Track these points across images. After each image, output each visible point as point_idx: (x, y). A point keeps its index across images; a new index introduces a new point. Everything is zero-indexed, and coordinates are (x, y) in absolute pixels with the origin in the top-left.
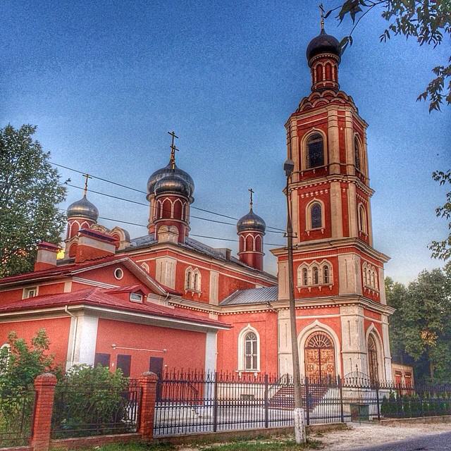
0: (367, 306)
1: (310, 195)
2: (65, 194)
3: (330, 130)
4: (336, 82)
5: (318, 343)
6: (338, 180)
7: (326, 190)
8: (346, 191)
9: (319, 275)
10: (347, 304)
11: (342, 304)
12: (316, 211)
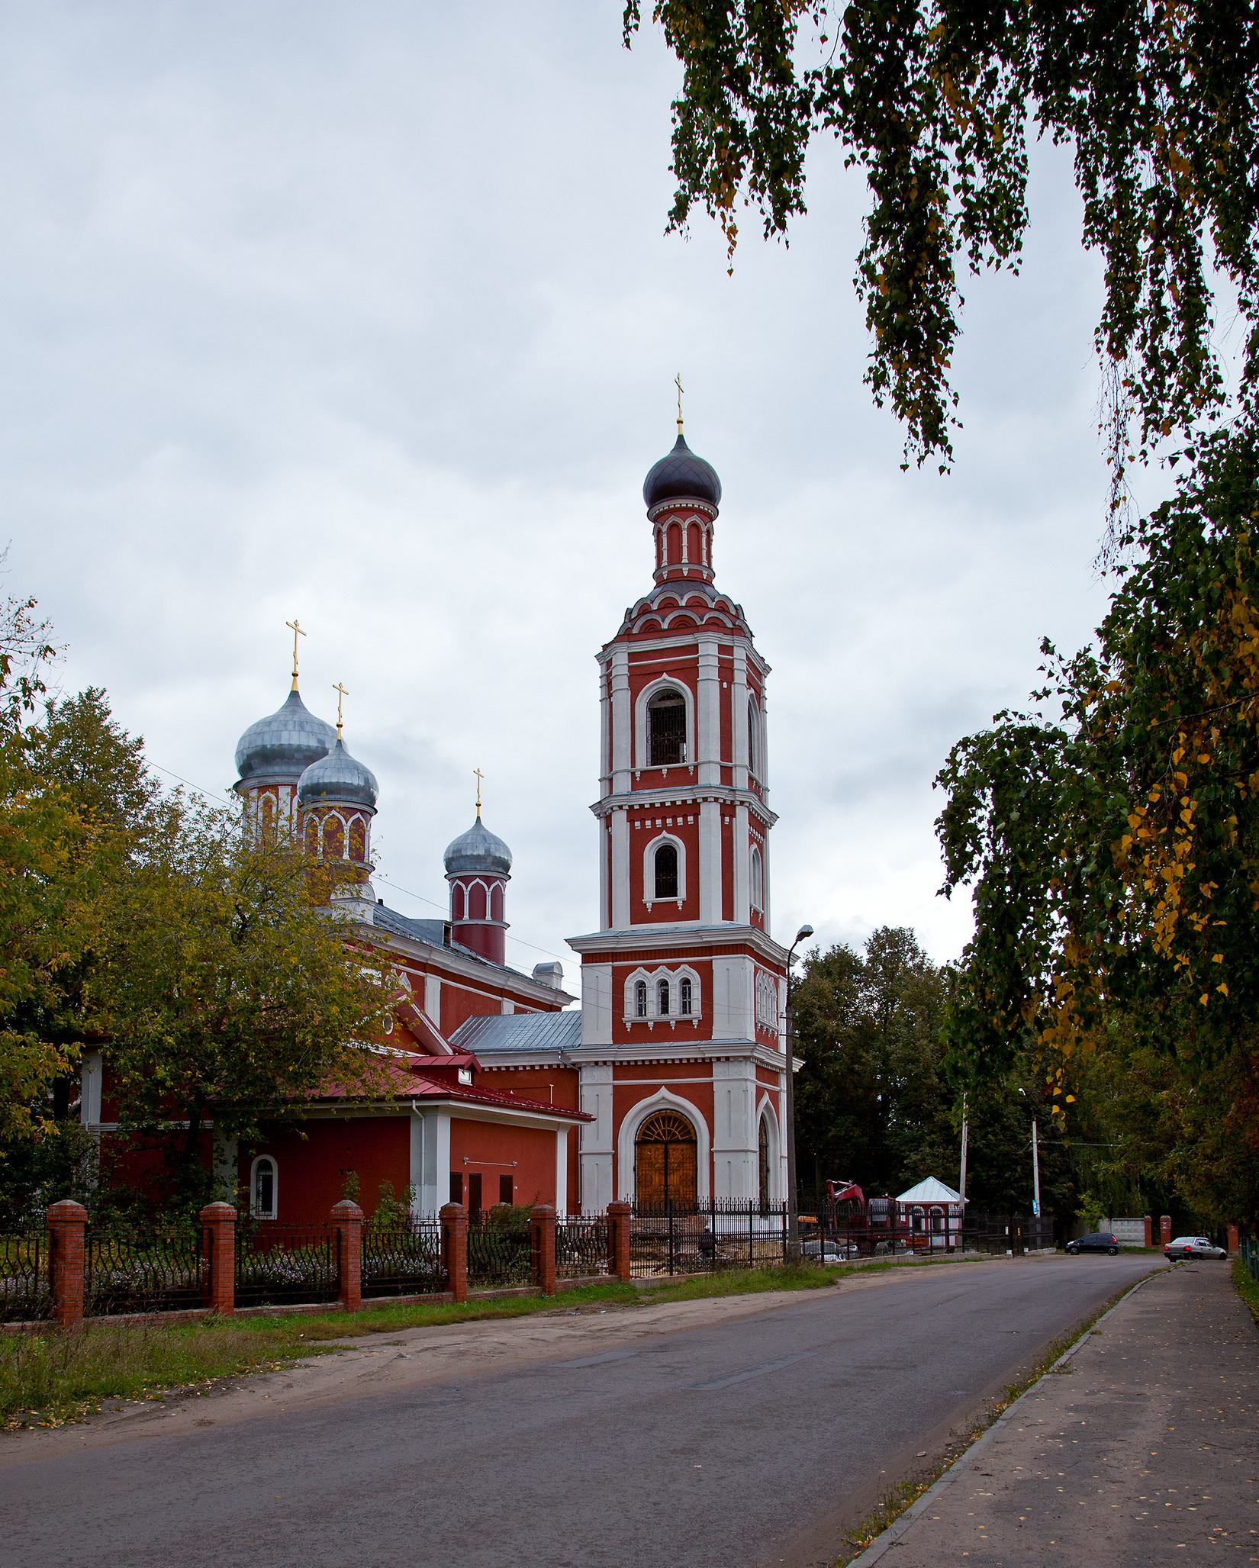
0: (762, 1061)
1: (654, 824)
2: (833, 128)
3: (700, 685)
4: (710, 567)
5: (663, 1131)
6: (716, 800)
7: (690, 819)
8: (731, 820)
9: (671, 997)
10: (727, 1059)
11: (718, 1059)
12: (666, 859)
